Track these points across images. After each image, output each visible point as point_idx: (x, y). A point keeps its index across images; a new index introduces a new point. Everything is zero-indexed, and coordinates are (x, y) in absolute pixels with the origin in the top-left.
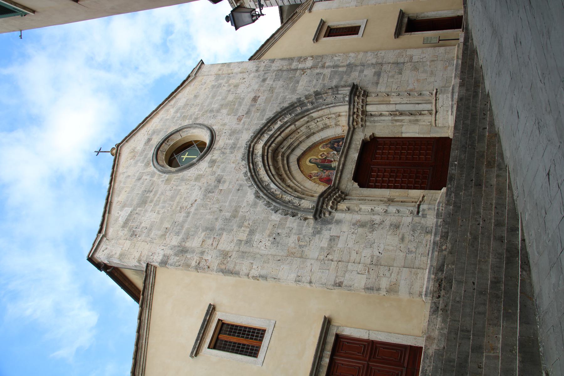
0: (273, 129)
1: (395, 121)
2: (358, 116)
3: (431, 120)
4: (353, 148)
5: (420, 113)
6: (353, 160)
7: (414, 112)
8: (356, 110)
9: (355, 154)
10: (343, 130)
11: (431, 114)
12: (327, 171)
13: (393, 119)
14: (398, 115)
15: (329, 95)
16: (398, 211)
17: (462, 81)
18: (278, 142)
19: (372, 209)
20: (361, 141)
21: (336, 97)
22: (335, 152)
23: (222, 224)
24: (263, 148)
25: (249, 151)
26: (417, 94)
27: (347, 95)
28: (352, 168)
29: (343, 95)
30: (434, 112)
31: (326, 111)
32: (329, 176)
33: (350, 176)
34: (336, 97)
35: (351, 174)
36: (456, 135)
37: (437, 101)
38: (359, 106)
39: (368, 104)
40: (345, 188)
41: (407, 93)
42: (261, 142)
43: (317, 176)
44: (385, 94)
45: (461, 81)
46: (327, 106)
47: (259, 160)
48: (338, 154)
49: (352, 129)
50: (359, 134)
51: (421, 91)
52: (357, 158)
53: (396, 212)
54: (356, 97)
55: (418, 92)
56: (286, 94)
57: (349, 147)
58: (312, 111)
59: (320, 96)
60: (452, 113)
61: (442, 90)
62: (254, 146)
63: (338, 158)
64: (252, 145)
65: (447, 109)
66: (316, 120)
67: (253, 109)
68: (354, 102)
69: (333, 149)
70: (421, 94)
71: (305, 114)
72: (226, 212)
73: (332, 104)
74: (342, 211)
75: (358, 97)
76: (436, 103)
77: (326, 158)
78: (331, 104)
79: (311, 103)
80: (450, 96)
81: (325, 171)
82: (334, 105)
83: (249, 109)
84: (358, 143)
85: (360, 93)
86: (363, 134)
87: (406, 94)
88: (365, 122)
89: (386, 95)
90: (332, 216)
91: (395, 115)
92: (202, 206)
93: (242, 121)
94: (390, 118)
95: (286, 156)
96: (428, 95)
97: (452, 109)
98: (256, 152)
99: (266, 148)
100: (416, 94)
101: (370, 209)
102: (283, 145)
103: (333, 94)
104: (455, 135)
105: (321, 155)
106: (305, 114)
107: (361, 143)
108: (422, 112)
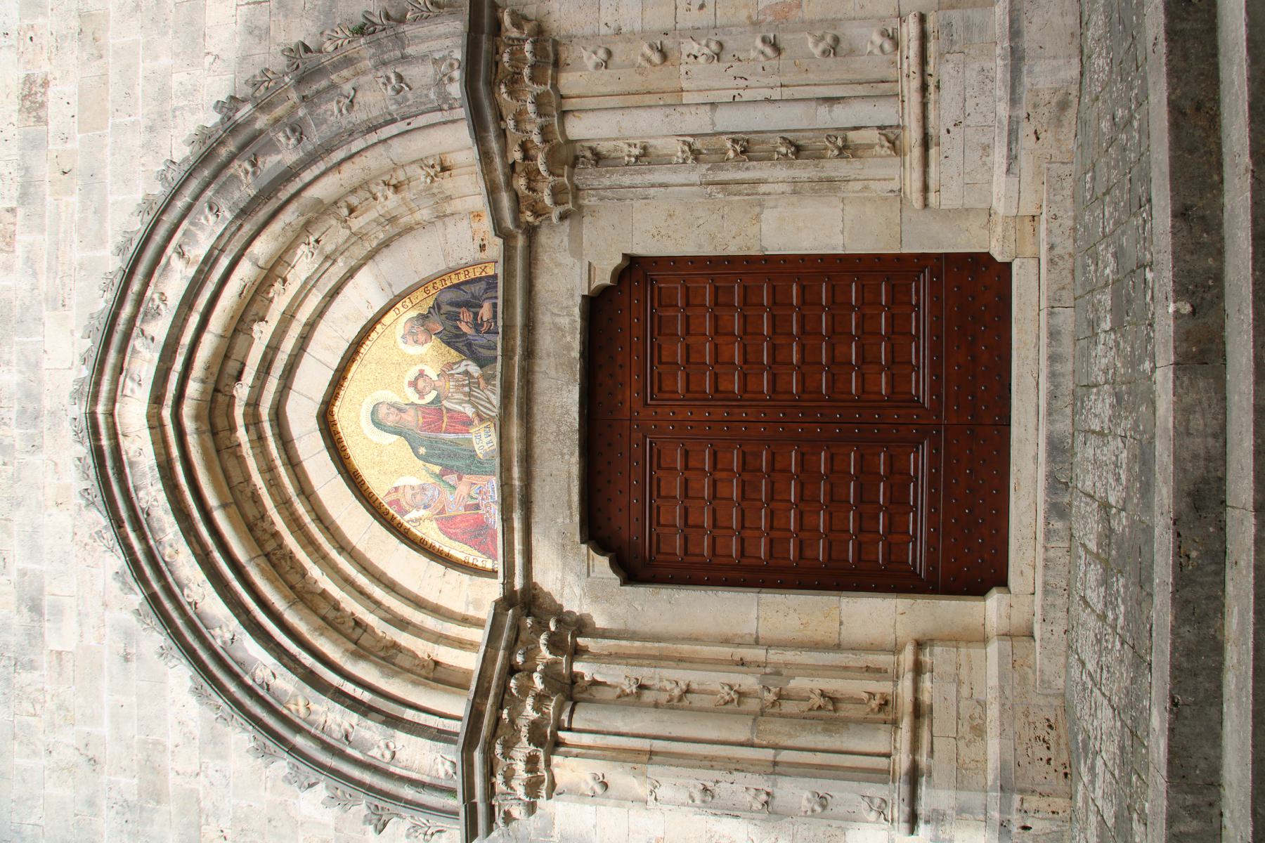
0: (162, 306)
1: (723, 190)
2: (533, 176)
3: (902, 179)
4: (548, 356)
5: (840, 142)
6: (564, 428)
7: (810, 134)
8: (517, 155)
9: (565, 394)
10: (478, 242)
11: (895, 146)
12: (460, 479)
13: (711, 177)
14: (731, 154)
15: (364, 73)
16: (823, 801)
17: (1194, 312)
18: (208, 368)
19: (705, 789)
20: (577, 311)
21: (400, 78)
22: (474, 369)
23: (122, 831)
24: (155, 424)
25: (98, 453)
26: (816, 45)
27: (451, 65)
28: (565, 476)
29: (435, 61)
30: (913, 135)
31: (373, 161)
32: (477, 507)
33: (568, 521)
34: (400, 78)
35: (570, 507)
36: (1182, 828)
37: (932, 96)
38: (529, 128)
39: (572, 111)
40: (559, 584)
41: (764, 40)
42: (132, 390)
43: (426, 507)
44: (648, 52)
45: (1186, 308)
46: (373, 138)
47: (152, 496)
48: (488, 379)
49: (520, 241)
50: (559, 265)
51: (834, 23)
52: (577, 416)
53: (813, 811)
54: (503, 89)
55: (818, 33)
56: (165, 61)
57: (530, 353)
58: (307, 176)
59: (324, 83)
60: (1009, 165)
61: (950, 24)
62: (111, 414)
63: (490, 403)
64: (101, 419)
65: (985, 140)
66: (342, 204)
67: (46, 170)
68: (500, 117)
69: (460, 345)
70: (836, 40)
71: (283, 195)
72: (116, 773)
73: (393, 121)
74: (576, 793)
75: (514, 81)
76: (924, 106)
77: (437, 400)
78: (387, 123)
79: (294, 131)
80: (999, 76)
81: (452, 479)
82: (401, 126)
83: (27, 169)
84: (564, 321)
85: (517, 58)
86: (578, 264)
87: (759, 44)
88: (575, 198)
89: (656, 58)
90: (541, 817)
91: (720, 159)
92: (14, 738)
93: (20, 250)
94: (696, 174)
95: (265, 410)
96: (876, 51)
97: (1009, 143)
98: (131, 454)
99: (166, 413)
100: (811, 45)
101: (695, 786)
102: (234, 357)
103: (384, 64)
104: (1175, 829)
105: (414, 384)
106: (283, 195)
107: (579, 320)
108: (852, 135)
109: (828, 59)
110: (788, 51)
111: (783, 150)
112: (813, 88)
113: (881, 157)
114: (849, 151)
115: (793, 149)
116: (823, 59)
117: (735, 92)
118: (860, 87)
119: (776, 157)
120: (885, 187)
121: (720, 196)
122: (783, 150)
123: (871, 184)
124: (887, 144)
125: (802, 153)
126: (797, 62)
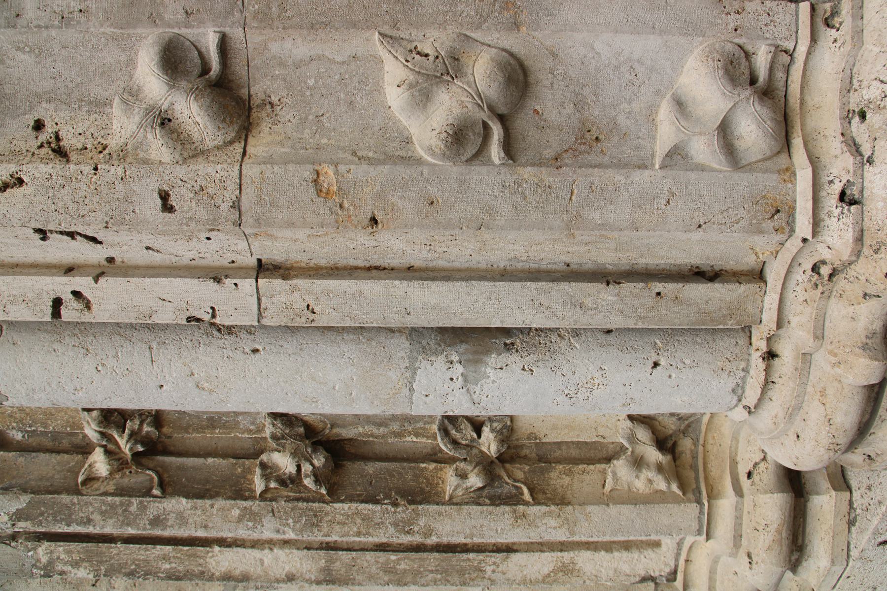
109: (478, 171)
110: (286, 114)
111: (284, 462)
112: (399, 287)
113: (633, 499)
114: (520, 471)
115: (319, 461)
116: (454, 170)
117: (63, 286)
118: (606, 295)
119: (259, 485)
120: (625, 568)
121: (83, 573)
122: (284, 462)
123: (585, 560)
124: (653, 455)
125: (353, 468)
126: (329, 175)
